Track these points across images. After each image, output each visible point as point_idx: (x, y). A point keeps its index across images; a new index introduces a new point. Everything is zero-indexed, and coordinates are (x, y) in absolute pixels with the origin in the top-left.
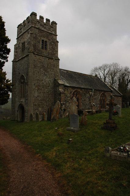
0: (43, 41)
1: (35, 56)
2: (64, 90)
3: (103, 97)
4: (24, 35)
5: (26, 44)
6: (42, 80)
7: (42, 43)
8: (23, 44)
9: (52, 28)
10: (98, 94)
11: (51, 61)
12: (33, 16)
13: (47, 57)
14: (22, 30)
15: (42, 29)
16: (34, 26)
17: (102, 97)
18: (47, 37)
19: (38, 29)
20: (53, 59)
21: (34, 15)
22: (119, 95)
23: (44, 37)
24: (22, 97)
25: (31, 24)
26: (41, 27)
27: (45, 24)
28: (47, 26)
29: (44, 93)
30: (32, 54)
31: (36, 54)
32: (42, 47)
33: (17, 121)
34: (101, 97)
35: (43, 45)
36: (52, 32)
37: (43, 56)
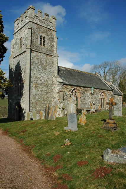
2: (63, 88)
5: (23, 39)
6: (40, 78)
9: (51, 24)
10: (98, 93)
11: (50, 58)
13: (46, 54)
15: (40, 24)
16: (32, 21)
26: (39, 22)
29: (42, 90)
36: (51, 27)
37: (41, 53)
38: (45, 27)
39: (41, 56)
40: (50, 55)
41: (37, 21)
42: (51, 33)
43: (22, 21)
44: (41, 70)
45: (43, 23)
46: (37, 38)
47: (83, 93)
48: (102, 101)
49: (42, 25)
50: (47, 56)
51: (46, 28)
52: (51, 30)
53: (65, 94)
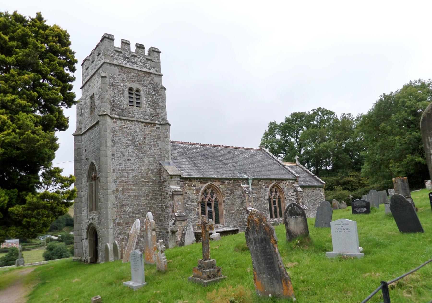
0: (131, 89)
1: (115, 122)
2: (181, 187)
3: (276, 192)
4: (92, 79)
5: (96, 97)
7: (129, 93)
8: (92, 97)
9: (149, 62)
10: (264, 188)
12: (106, 41)
13: (142, 122)
14: (89, 69)
15: (126, 66)
16: (108, 61)
17: (274, 194)
18: (140, 81)
19: (118, 66)
20: (155, 124)
21: (109, 38)
22: (316, 183)
23: (133, 82)
24: (94, 208)
25: (103, 57)
26: (125, 62)
27: (133, 56)
28: (139, 58)
30: (108, 119)
31: (116, 118)
32: (130, 101)
33: (86, 261)
34: (271, 192)
35: (132, 98)
36: (149, 69)
37: (132, 121)
38: (137, 70)
39: (132, 128)
40: (152, 123)
41: (119, 61)
42: (152, 80)
43: (93, 62)
44: (134, 155)
45: (133, 63)
46: (121, 94)
47: (229, 192)
48: (275, 203)
49: (130, 67)
50: (145, 126)
51: (141, 71)
52: (152, 73)
53: (189, 198)
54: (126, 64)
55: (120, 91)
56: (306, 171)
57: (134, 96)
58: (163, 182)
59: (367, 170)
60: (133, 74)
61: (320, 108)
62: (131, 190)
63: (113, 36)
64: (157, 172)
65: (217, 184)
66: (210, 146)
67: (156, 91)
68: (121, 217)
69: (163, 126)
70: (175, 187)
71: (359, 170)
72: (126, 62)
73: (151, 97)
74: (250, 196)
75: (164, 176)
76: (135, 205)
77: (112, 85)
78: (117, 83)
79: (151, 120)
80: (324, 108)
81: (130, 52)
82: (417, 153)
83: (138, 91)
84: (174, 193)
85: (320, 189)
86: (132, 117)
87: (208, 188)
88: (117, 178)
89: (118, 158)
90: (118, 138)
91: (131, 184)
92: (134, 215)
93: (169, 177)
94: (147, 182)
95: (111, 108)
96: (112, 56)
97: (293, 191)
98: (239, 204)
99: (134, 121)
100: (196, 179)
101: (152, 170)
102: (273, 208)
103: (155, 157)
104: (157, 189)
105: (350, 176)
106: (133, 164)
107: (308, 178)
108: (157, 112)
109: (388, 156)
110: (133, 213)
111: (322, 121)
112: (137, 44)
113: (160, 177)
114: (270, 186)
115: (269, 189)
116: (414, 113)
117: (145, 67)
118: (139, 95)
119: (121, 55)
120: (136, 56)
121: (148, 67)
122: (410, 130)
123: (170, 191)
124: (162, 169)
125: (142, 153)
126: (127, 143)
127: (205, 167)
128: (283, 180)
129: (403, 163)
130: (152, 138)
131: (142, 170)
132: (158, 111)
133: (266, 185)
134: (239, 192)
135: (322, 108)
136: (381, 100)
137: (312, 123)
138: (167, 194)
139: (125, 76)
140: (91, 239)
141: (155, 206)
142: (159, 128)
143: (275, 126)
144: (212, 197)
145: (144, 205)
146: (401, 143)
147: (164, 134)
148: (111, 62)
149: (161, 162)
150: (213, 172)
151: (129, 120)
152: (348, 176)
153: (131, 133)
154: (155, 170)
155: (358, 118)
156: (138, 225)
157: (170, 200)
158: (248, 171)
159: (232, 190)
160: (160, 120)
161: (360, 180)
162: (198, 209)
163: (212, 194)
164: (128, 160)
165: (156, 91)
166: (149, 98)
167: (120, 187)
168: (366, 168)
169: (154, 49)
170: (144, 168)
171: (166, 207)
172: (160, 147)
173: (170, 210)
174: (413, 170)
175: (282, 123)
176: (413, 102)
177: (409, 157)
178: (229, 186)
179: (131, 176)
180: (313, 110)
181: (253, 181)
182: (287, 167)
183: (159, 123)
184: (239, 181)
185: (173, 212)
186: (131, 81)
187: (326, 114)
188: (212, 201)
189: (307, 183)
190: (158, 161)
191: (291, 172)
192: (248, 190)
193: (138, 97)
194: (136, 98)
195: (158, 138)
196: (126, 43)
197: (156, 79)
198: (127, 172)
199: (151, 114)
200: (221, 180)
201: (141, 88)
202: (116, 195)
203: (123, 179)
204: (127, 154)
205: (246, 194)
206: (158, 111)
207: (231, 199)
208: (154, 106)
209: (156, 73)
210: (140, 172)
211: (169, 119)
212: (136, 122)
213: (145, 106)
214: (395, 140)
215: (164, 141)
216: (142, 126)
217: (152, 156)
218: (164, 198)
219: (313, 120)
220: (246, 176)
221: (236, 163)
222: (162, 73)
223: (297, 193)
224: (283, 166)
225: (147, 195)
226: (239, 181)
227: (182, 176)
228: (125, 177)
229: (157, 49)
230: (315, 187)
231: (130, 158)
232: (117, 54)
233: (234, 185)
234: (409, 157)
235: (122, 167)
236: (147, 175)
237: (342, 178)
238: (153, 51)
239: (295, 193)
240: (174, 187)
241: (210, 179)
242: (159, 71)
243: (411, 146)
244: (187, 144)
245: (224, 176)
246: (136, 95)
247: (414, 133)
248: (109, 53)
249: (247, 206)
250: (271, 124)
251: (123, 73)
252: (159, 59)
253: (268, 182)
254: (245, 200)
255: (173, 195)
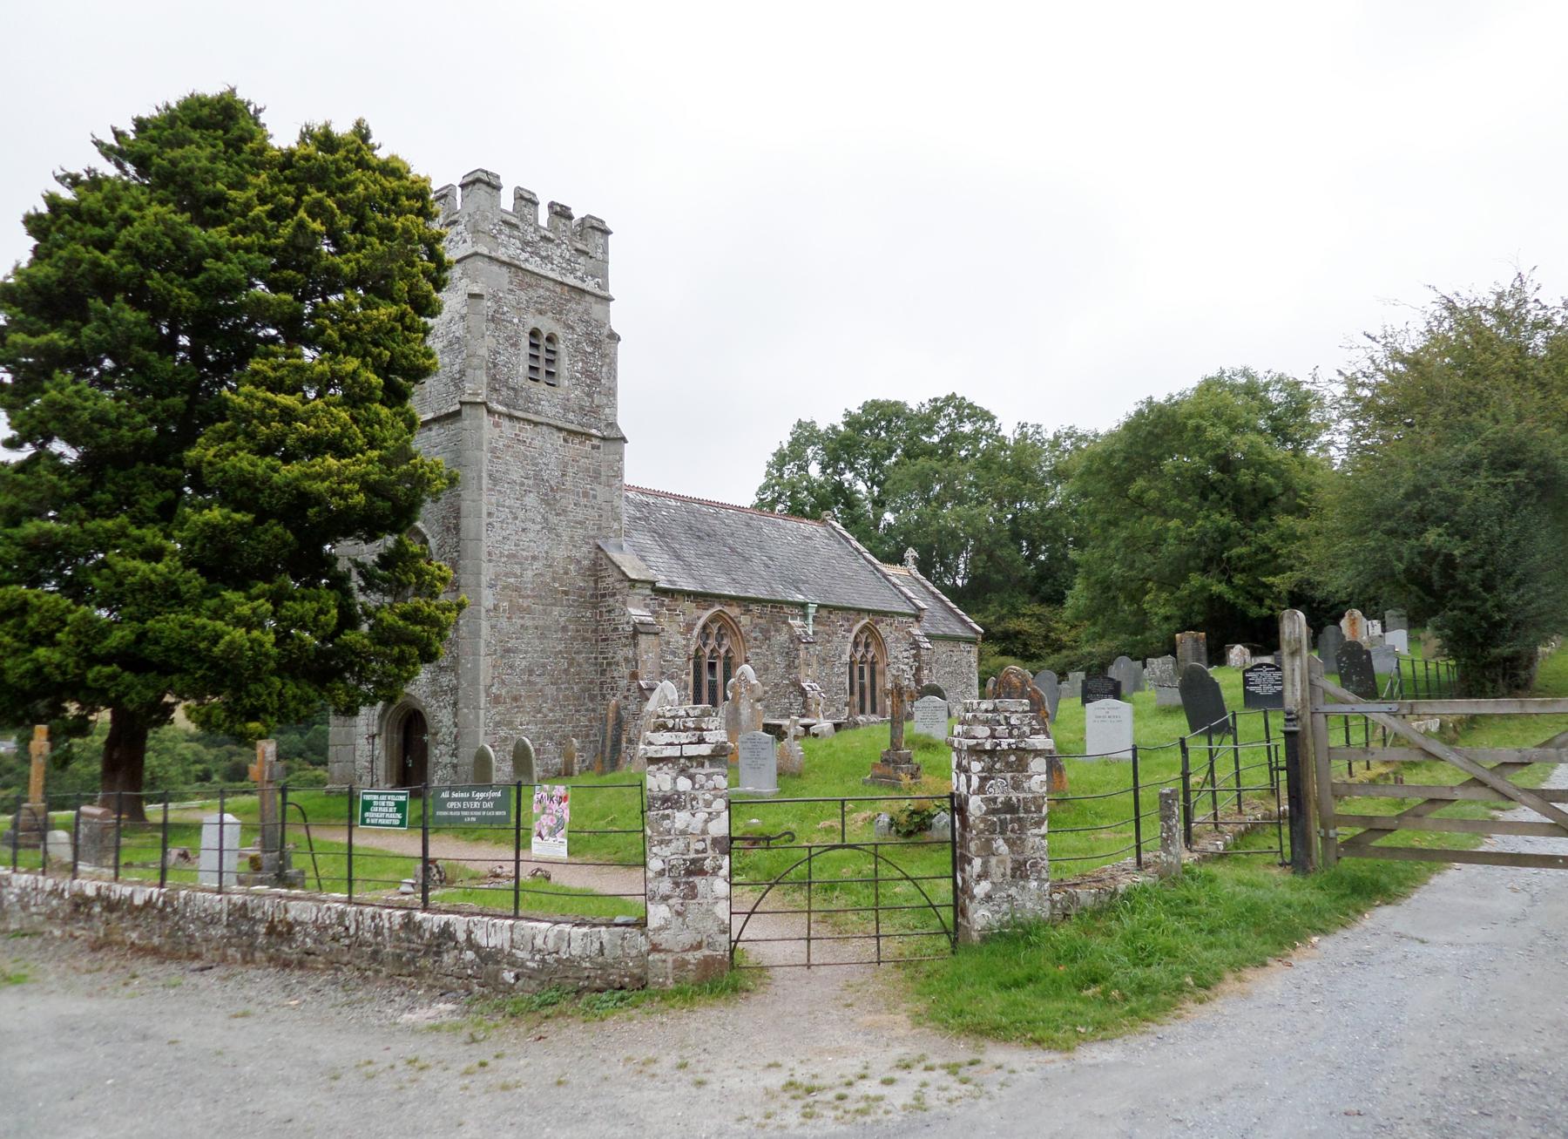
0: (534, 333)
1: (497, 425)
2: (654, 612)
3: (867, 646)
7: (532, 345)
9: (582, 260)
10: (841, 632)
12: (481, 192)
13: (560, 429)
15: (529, 267)
16: (485, 251)
17: (861, 649)
20: (590, 436)
21: (488, 184)
22: (959, 631)
23: (541, 312)
26: (524, 256)
27: (545, 238)
28: (558, 245)
31: (500, 414)
32: (531, 367)
34: (856, 644)
35: (537, 357)
37: (536, 424)
39: (536, 443)
40: (582, 434)
42: (587, 312)
45: (543, 258)
46: (512, 345)
47: (760, 636)
48: (861, 677)
50: (565, 440)
52: (588, 293)
54: (527, 260)
55: (511, 338)
56: (933, 593)
57: (542, 354)
58: (603, 596)
59: (1082, 602)
60: (541, 291)
61: (954, 396)
62: (528, 610)
63: (498, 177)
64: (589, 569)
65: (733, 611)
66: (700, 502)
67: (595, 344)
68: (503, 682)
69: (608, 443)
70: (639, 612)
71: (1057, 599)
72: (527, 255)
73: (582, 360)
74: (811, 650)
75: (611, 581)
76: (536, 651)
77: (493, 320)
78: (504, 314)
79: (579, 424)
80: (964, 398)
81: (537, 229)
82: (1215, 571)
83: (551, 339)
84: (641, 628)
85: (967, 647)
86: (536, 413)
87: (712, 622)
88: (497, 576)
89: (502, 522)
90: (503, 468)
91: (529, 596)
92: (532, 679)
93: (627, 584)
94: (566, 593)
95: (489, 384)
96: (494, 237)
97: (906, 646)
98: (781, 671)
99: (542, 424)
100: (688, 594)
101: (579, 562)
102: (857, 689)
103: (587, 528)
104: (588, 614)
105: (1024, 615)
106: (533, 542)
107: (940, 614)
108: (596, 402)
109: (1143, 570)
110: (531, 672)
111: (954, 438)
112: (518, 189)
113: (596, 582)
114: (856, 629)
115: (852, 638)
116: (1221, 463)
117: (573, 271)
118: (554, 352)
119: (516, 233)
120: (551, 241)
121: (579, 274)
122: (1207, 504)
123: (628, 623)
124: (604, 561)
125: (557, 515)
126: (522, 484)
127: (701, 563)
128: (885, 614)
129: (1178, 594)
130: (581, 475)
131: (554, 559)
132: (597, 400)
133: (846, 625)
134: (782, 638)
135: (959, 396)
136: (1140, 413)
137: (926, 439)
138: (616, 629)
139: (523, 296)
140: (392, 738)
141: (580, 658)
142: (598, 447)
143: (811, 435)
144: (720, 646)
145: (556, 654)
146: (1178, 538)
147: (610, 467)
148: (493, 254)
149: (600, 543)
150: (722, 579)
151: (529, 421)
152: (1018, 616)
153: (534, 458)
154: (586, 563)
155: (1057, 437)
156: (673, 694)
157: (625, 646)
158: (805, 582)
159: (768, 631)
160: (602, 425)
161: (1050, 629)
162: (687, 674)
163: (720, 637)
164: (524, 530)
165: (595, 344)
166: (577, 362)
167: (503, 601)
168: (1078, 595)
169: (595, 224)
170: (560, 553)
171: (609, 664)
172: (600, 500)
173: (625, 670)
174: (1201, 614)
175: (834, 428)
176: (1221, 431)
177: (1196, 580)
178: (760, 621)
179: (530, 573)
180: (936, 400)
181: (817, 611)
182: (894, 579)
183: (599, 434)
184: (786, 610)
185: (634, 676)
186: (537, 310)
187: (969, 417)
188: (718, 657)
189: (938, 629)
190: (594, 537)
191: (906, 596)
192: (806, 633)
193: (550, 356)
194: (547, 360)
195: (596, 476)
196: (525, 199)
197: (597, 309)
198: (521, 564)
199: (581, 408)
200: (744, 602)
201: (559, 331)
202: (493, 622)
203: (512, 580)
204: (521, 514)
205: (802, 646)
206: (597, 400)
207: (764, 655)
208: (588, 386)
209: (598, 291)
210: (550, 566)
211: (625, 425)
212: (545, 428)
213: (566, 383)
214: (1168, 529)
215: (610, 486)
216: (558, 438)
217: (579, 523)
218: (604, 640)
219: (929, 431)
220: (800, 598)
221: (771, 559)
222: (612, 292)
223: (919, 651)
224: (885, 576)
225: (564, 629)
226: (786, 610)
227: (657, 585)
228: (516, 576)
229: (602, 221)
230: (956, 639)
231: (529, 525)
232: (507, 230)
233: (772, 621)
234: (1196, 580)
235: (508, 547)
236: (566, 573)
237: (1001, 618)
238: (593, 227)
239: (914, 652)
240: (638, 612)
241: (719, 597)
242: (605, 287)
243: (1203, 549)
244: (642, 493)
245: (751, 594)
246: (548, 351)
247: (1216, 516)
248: (487, 226)
249: (802, 676)
250: (800, 425)
251: (521, 286)
252: (605, 252)
253: (853, 616)
254: (797, 661)
255: (636, 633)
